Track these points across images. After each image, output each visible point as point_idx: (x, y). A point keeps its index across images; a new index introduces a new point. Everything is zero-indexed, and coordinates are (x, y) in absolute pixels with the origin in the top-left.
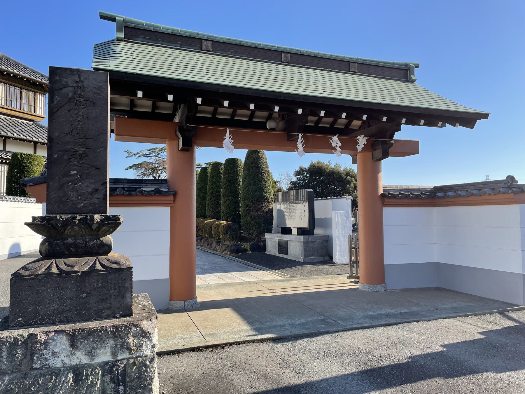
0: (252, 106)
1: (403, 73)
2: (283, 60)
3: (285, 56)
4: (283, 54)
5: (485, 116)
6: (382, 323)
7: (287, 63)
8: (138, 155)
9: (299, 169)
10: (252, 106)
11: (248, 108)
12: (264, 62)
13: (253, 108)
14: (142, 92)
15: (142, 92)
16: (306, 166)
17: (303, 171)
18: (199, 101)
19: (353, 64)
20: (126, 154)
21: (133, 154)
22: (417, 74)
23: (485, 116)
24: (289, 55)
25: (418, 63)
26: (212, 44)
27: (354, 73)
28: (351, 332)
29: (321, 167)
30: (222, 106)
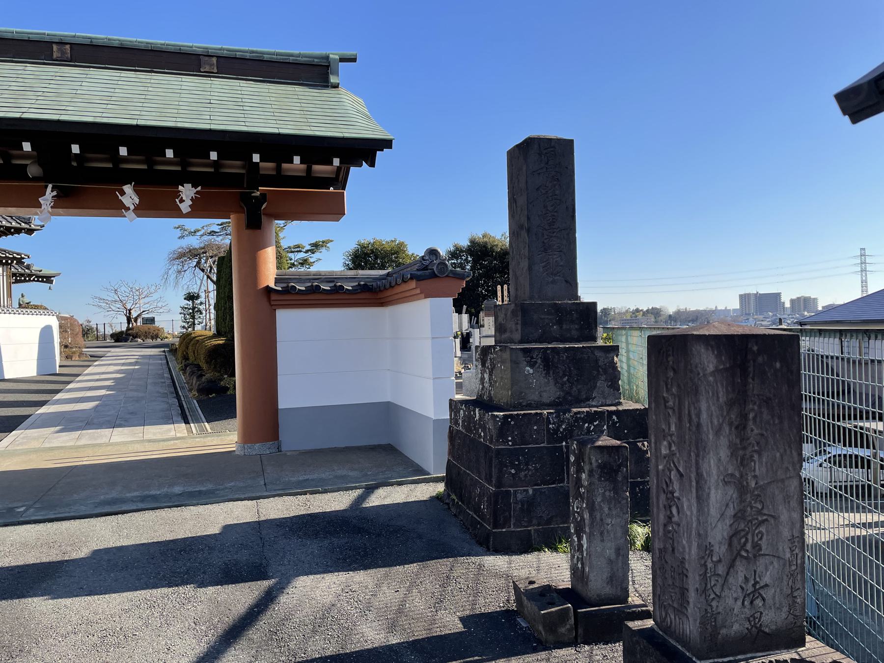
0: (214, 156)
1: (315, 73)
2: (55, 56)
3: (59, 50)
4: (55, 47)
5: (387, 144)
6: (135, 508)
7: (63, 61)
8: (198, 234)
9: (452, 249)
10: (214, 156)
11: (331, 163)
12: (13, 62)
13: (78, 152)
14: (299, 157)
15: (299, 157)
16: (465, 243)
17: (461, 251)
18: (123, 151)
19: (207, 58)
20: (179, 233)
21: (190, 233)
22: (342, 74)
23: (387, 144)
24: (68, 47)
25: (354, 53)
26: (71, 48)
27: (209, 75)
28: (104, 518)
29: (486, 243)
30: (291, 161)
